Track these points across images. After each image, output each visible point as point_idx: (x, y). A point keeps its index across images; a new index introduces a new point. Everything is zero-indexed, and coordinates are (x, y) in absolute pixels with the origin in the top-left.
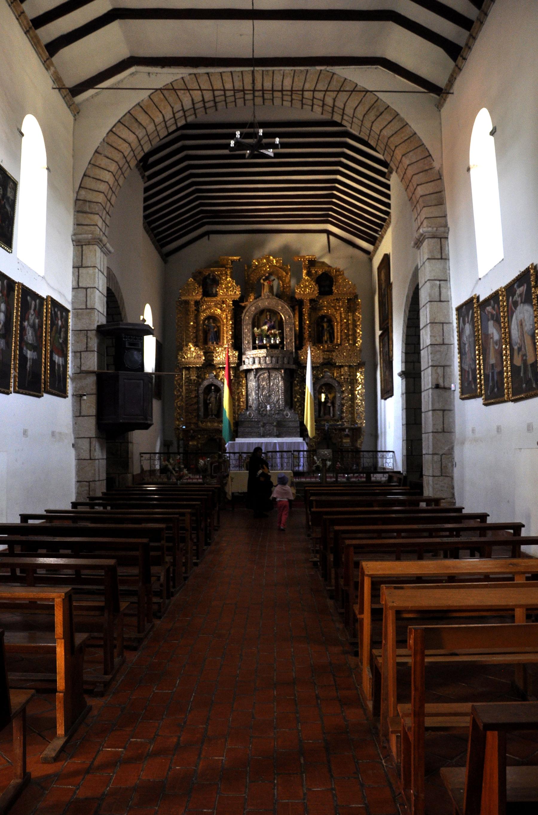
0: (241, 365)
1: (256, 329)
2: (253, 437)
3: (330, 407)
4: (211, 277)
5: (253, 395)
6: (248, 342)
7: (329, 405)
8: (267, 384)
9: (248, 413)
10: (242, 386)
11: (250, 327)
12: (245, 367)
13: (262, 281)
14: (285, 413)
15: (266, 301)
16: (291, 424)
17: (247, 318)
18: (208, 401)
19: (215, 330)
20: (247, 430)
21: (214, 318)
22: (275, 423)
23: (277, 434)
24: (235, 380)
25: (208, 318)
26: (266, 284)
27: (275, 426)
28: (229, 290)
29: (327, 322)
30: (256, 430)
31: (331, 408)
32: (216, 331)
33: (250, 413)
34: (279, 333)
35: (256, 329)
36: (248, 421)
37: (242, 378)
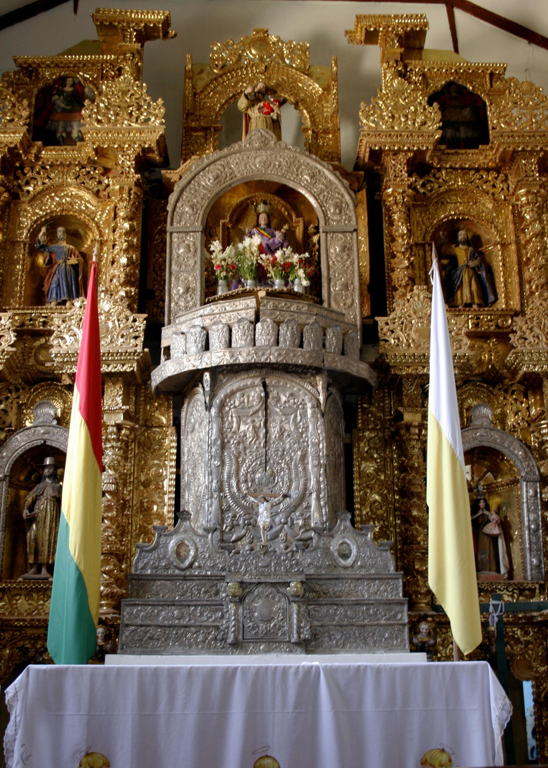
0: (157, 363)
1: (216, 245)
2: (188, 648)
3: (494, 539)
4: (68, 89)
5: (199, 482)
6: (187, 290)
7: (493, 529)
8: (256, 430)
9: (172, 544)
10: (162, 456)
11: (195, 239)
12: (167, 370)
13: (242, 103)
14: (334, 546)
15: (251, 158)
16: (365, 591)
17: (185, 216)
18: (26, 513)
19: (73, 261)
20: (163, 616)
21: (65, 225)
22: (294, 587)
23: (306, 634)
24: (132, 429)
25: (53, 222)
26: (255, 113)
27: (296, 598)
28: (125, 120)
29: (467, 242)
30: (207, 617)
31: (501, 543)
32: (75, 267)
33: (180, 545)
34: (301, 260)
35: (216, 245)
36: (171, 578)
37: (161, 426)
